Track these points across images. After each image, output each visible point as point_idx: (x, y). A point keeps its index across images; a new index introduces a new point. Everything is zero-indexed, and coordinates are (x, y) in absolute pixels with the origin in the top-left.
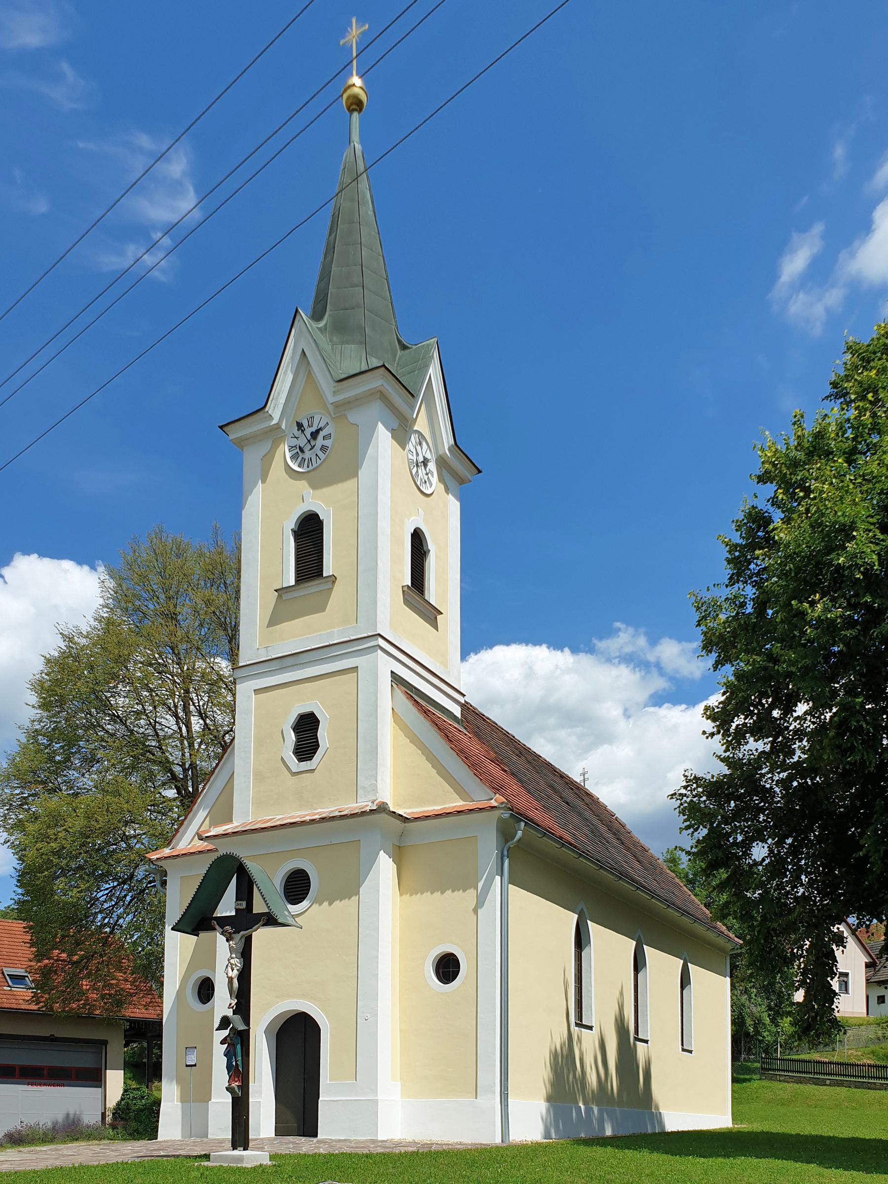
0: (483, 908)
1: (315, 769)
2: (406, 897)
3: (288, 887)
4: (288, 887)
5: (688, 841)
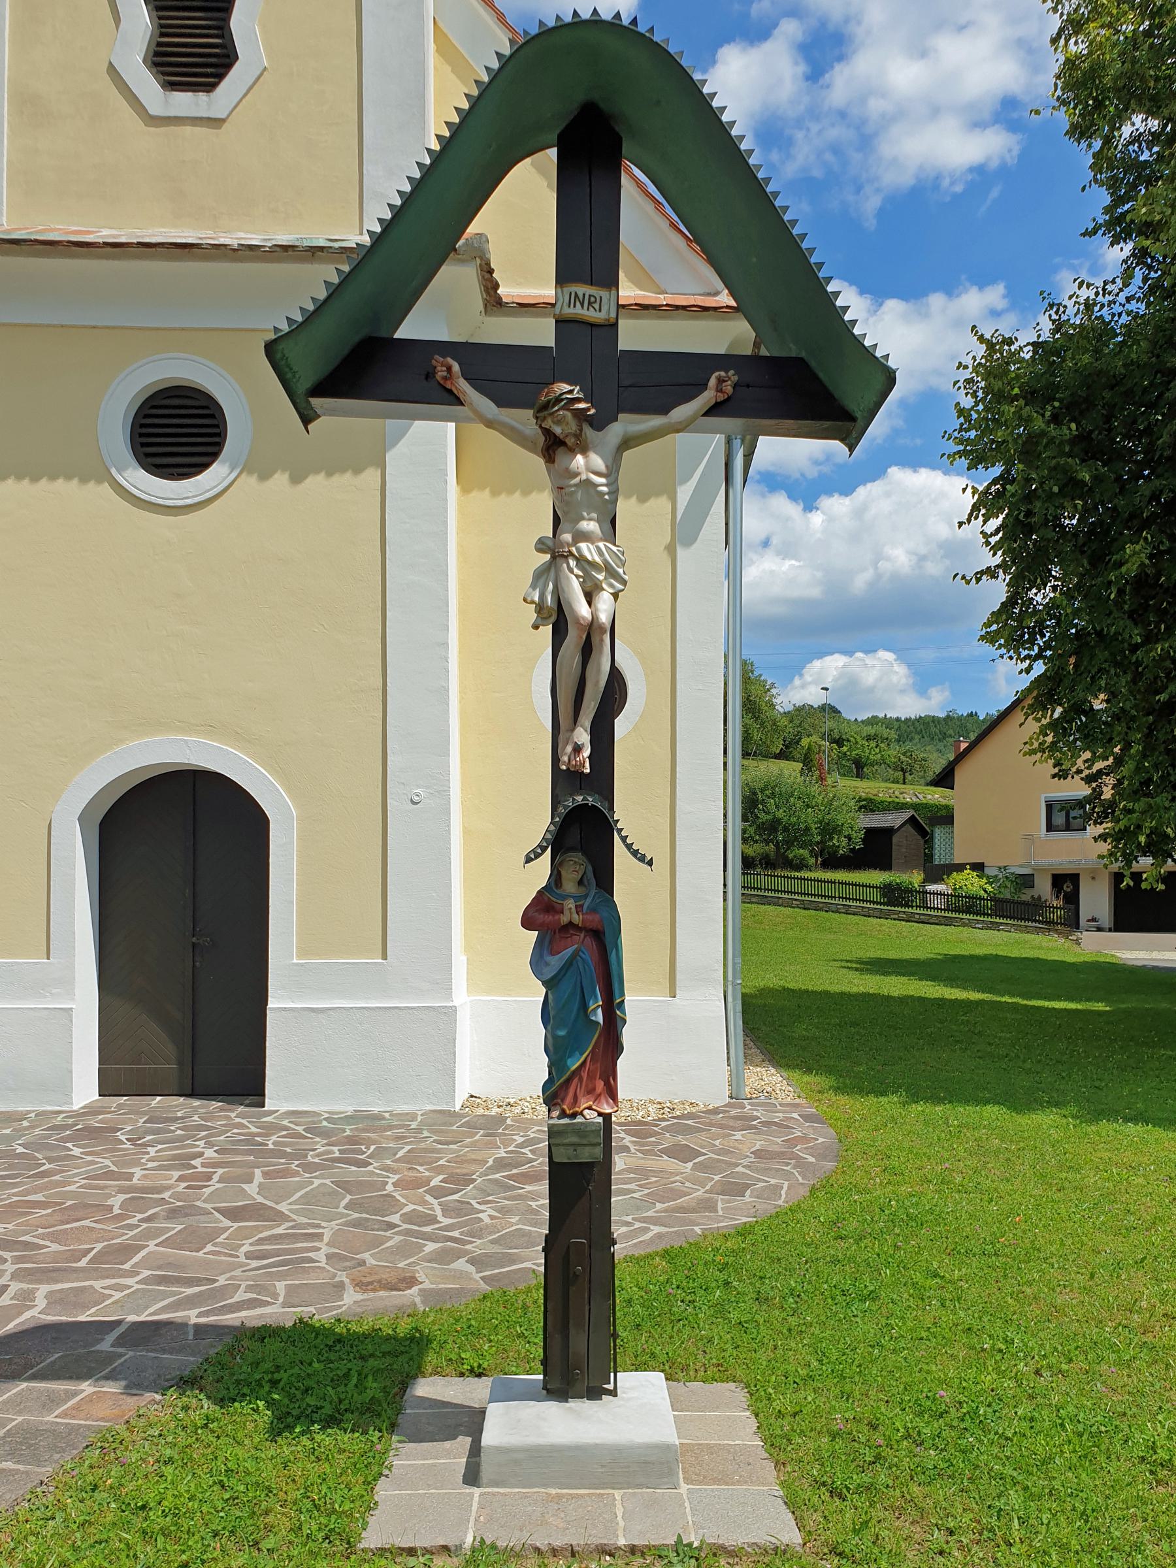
0: (695, 546)
1: (223, 121)
2: (482, 497)
3: (144, 430)
4: (144, 430)
5: (819, 535)
